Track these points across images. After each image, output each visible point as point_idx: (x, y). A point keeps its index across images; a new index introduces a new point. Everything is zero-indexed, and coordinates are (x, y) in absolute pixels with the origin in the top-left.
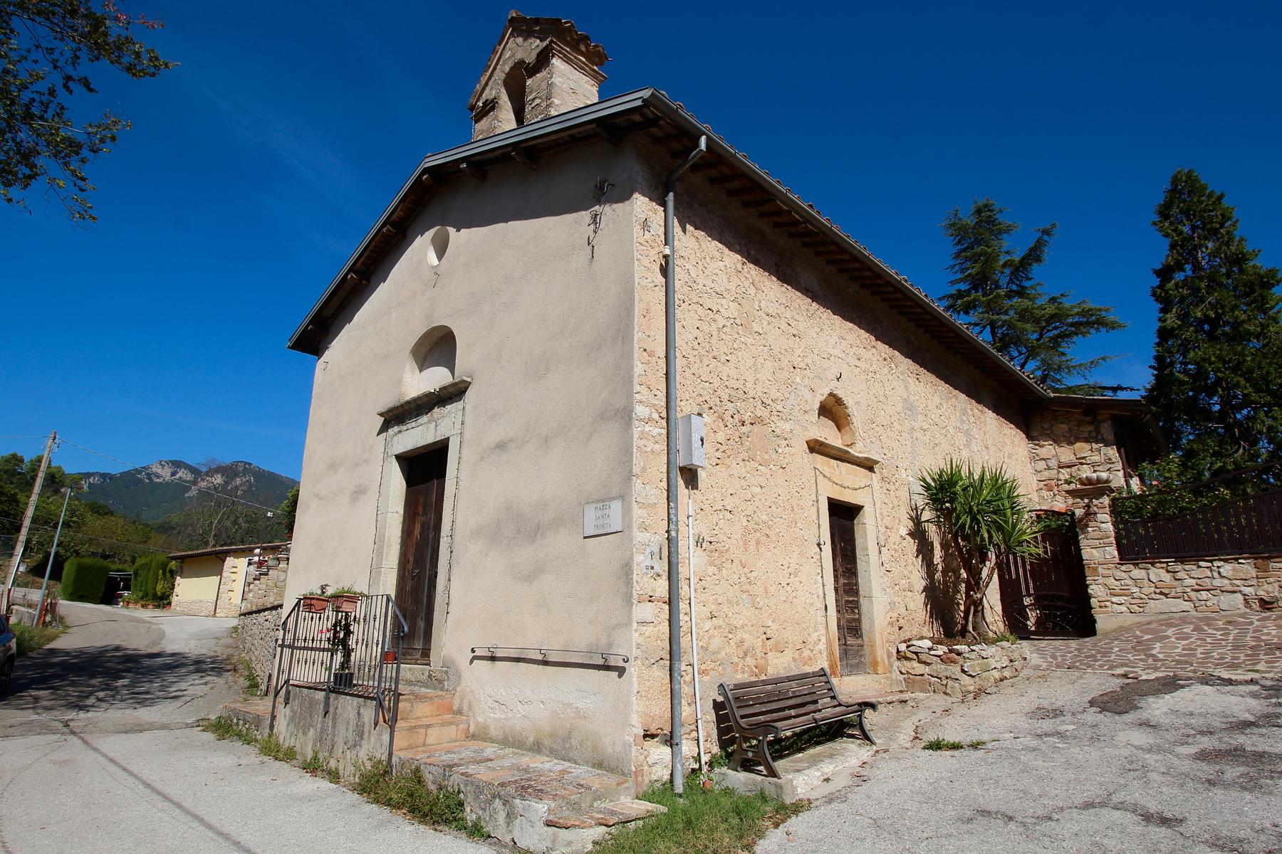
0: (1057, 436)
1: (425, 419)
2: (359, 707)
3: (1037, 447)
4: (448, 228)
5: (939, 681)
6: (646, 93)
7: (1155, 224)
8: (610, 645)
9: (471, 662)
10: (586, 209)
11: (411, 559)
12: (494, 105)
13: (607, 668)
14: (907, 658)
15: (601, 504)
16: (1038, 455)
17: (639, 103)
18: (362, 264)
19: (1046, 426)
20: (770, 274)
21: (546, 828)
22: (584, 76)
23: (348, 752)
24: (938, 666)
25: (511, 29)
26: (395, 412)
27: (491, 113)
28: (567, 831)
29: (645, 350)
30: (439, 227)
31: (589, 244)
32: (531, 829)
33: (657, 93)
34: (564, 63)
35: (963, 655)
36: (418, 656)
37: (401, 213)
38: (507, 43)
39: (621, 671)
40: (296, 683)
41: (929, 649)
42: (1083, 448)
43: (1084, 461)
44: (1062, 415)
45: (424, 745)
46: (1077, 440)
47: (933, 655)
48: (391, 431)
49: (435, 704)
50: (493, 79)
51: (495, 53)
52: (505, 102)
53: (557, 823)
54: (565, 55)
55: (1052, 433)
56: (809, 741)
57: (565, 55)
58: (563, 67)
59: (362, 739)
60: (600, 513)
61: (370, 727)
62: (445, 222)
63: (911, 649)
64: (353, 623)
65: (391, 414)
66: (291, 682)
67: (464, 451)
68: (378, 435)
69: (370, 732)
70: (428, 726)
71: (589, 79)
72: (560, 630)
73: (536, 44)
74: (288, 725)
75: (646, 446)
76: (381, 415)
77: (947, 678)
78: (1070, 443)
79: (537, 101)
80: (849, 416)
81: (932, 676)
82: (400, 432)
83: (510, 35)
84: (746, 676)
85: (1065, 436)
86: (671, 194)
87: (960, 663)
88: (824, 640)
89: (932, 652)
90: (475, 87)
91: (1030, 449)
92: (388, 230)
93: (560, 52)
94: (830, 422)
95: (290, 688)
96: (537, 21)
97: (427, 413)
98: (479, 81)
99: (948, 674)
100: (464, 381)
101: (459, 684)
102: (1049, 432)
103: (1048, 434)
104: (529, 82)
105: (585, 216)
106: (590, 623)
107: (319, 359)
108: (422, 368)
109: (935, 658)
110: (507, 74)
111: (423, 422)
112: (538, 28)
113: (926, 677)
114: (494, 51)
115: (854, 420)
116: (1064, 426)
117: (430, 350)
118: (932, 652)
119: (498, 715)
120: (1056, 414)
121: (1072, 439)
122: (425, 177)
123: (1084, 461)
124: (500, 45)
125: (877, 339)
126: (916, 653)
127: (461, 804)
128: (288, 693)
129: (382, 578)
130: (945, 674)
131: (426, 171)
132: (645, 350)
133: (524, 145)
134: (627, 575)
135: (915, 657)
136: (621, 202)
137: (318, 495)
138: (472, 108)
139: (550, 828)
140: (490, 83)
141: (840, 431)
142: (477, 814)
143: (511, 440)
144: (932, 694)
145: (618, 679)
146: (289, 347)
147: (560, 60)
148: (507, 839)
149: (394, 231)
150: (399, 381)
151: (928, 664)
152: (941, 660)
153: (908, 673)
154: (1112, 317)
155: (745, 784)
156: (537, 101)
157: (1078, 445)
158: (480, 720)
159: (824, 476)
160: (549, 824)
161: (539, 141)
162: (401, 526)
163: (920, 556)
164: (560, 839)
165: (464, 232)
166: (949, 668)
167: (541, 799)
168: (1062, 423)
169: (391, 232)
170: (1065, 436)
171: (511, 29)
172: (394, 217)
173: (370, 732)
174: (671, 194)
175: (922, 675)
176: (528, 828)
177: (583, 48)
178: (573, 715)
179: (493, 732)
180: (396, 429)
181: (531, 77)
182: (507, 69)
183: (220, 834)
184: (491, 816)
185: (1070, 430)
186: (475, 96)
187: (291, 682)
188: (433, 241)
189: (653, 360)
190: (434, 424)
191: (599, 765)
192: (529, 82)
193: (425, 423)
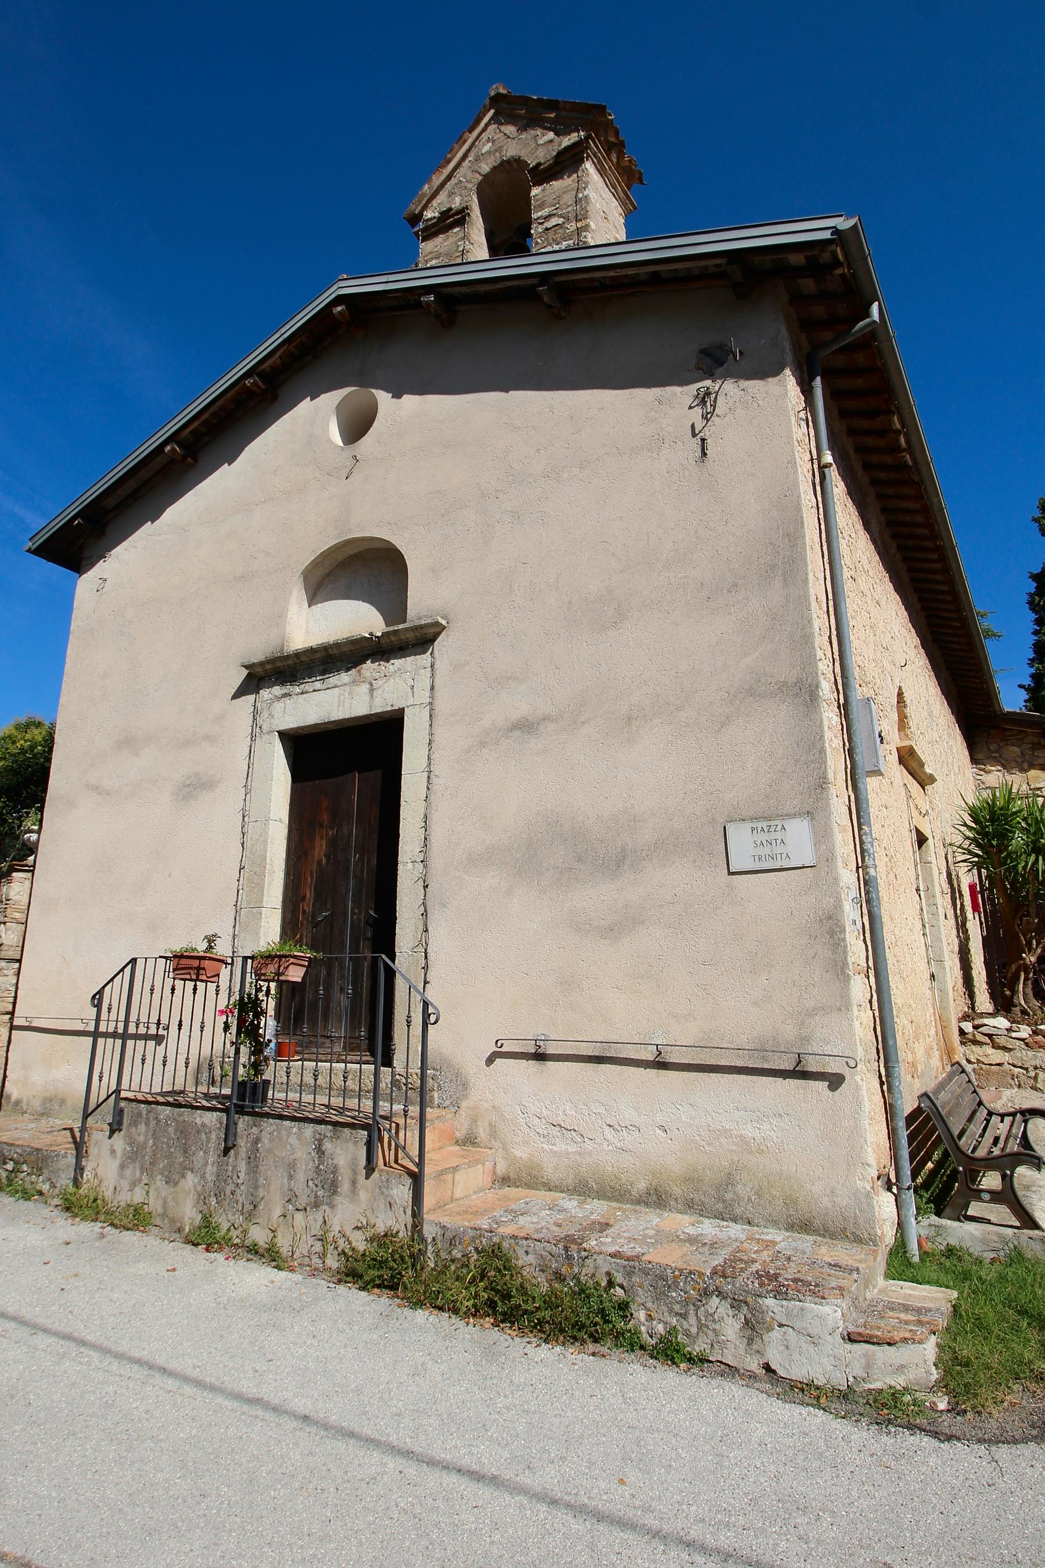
0: (1007, 761)
1: (344, 677)
2: (320, 1141)
3: (982, 773)
4: (373, 391)
5: (1025, 1072)
6: (843, 223)
7: (1035, 520)
8: (805, 1039)
9: (490, 1061)
10: (683, 382)
11: (309, 894)
12: (464, 218)
13: (800, 1073)
14: (975, 1042)
15: (764, 824)
16: (983, 783)
17: (827, 235)
18: (191, 432)
19: (993, 747)
21: (849, 1346)
23: (299, 1216)
24: (1023, 1051)
25: (492, 112)
26: (279, 664)
27: (456, 230)
28: (892, 1349)
30: (353, 388)
31: (694, 435)
32: (811, 1348)
36: (338, 1048)
37: (279, 360)
38: (484, 130)
39: (835, 1081)
40: (130, 1095)
41: (1007, 1029)
42: (1039, 777)
43: (1038, 792)
44: (1013, 735)
45: (452, 1200)
46: (1032, 766)
47: (1014, 1038)
48: (265, 694)
49: (437, 1131)
50: (453, 181)
51: (461, 142)
52: (477, 216)
53: (871, 1336)
54: (599, 161)
55: (1001, 756)
57: (599, 161)
58: (595, 177)
59: (335, 1193)
60: (763, 837)
61: (355, 1172)
62: (365, 379)
63: (982, 1029)
64: (265, 998)
65: (268, 667)
66: (123, 1094)
67: (438, 730)
68: (236, 696)
69: (354, 1182)
70: (455, 1169)
72: (689, 1014)
73: (546, 138)
74: (123, 1167)
76: (246, 667)
77: (1036, 1068)
78: (1023, 770)
79: (554, 221)
81: (1014, 1066)
82: (285, 695)
83: (489, 121)
85: (1016, 761)
86: (818, 378)
89: (1014, 1035)
90: (421, 187)
91: (974, 775)
92: (255, 383)
93: (595, 156)
95: (123, 1104)
96: (552, 105)
97: (348, 670)
98: (428, 180)
99: (1038, 1063)
100: (437, 624)
101: (466, 1096)
102: (998, 755)
103: (995, 757)
104: (535, 191)
105: (682, 395)
106: (756, 1004)
107: (80, 577)
108: (312, 601)
109: (1018, 1043)
110: (486, 177)
111: (339, 683)
112: (553, 115)
113: (1007, 1067)
114: (461, 140)
115: (911, 724)
116: (1016, 749)
117: (328, 575)
118: (1014, 1035)
119: (560, 1146)
120: (1006, 733)
121: (1025, 765)
122: (339, 309)
123: (1038, 792)
124: (470, 132)
126: (990, 1036)
127: (623, 1307)
128: (119, 1113)
129: (263, 924)
130: (1033, 1063)
131: (339, 300)
133: (449, 290)
134: (832, 933)
135: (987, 1040)
136: (761, 379)
137: (97, 788)
138: (415, 219)
139: (856, 1347)
140: (448, 186)
142: (666, 1323)
143: (546, 718)
144: (1016, 1089)
145: (830, 1093)
146: (29, 551)
148: (754, 1364)
149: (263, 387)
150: (281, 617)
151: (1005, 1049)
152: (1027, 1044)
153: (979, 1061)
154: (986, 624)
155: (984, 1241)
156: (554, 221)
157: (1033, 773)
158: (518, 1153)
160: (851, 1338)
161: (457, 289)
162: (285, 841)
164: (880, 1363)
165: (410, 401)
166: (1039, 1055)
167: (824, 1298)
168: (1013, 745)
169: (259, 387)
170: (1016, 761)
171: (492, 112)
172: (263, 367)
173: (354, 1182)
174: (818, 378)
176: (804, 1345)
178: (734, 1148)
179: (550, 1171)
180: (277, 690)
181: (540, 184)
182: (486, 168)
183: (212, 1388)
184: (701, 1327)
185: (1022, 754)
186: (420, 201)
187: (123, 1094)
188: (340, 409)
190: (365, 687)
191: (804, 1226)
192: (535, 191)
193: (345, 685)
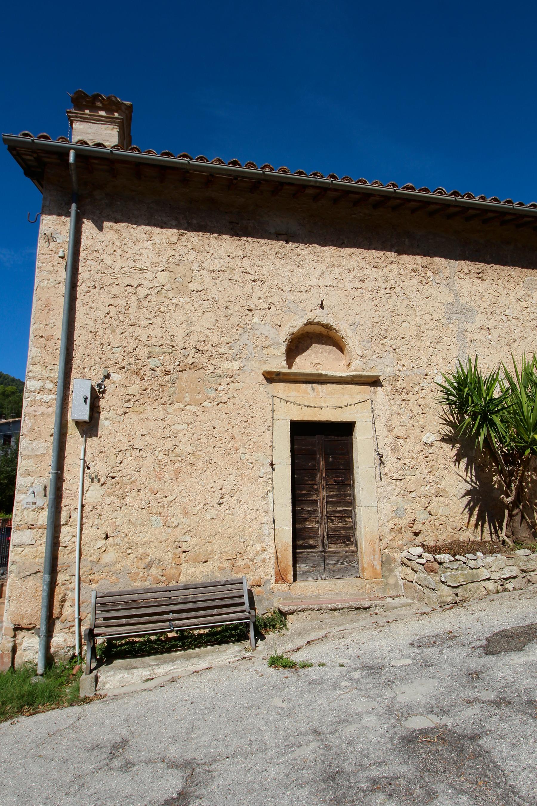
20: (220, 233)
22: (103, 126)
29: (42, 337)
33: (6, 137)
34: (82, 123)
35: (444, 565)
54: (81, 118)
56: (208, 641)
57: (81, 118)
58: (82, 127)
71: (107, 126)
75: (36, 411)
80: (343, 338)
84: (148, 583)
87: (439, 573)
88: (271, 550)
93: (76, 117)
94: (328, 347)
125: (400, 252)
132: (42, 337)
141: (343, 353)
147: (78, 123)
159: (287, 402)
163: (465, 461)
175: (412, 582)
177: (99, 104)
189: (51, 343)
